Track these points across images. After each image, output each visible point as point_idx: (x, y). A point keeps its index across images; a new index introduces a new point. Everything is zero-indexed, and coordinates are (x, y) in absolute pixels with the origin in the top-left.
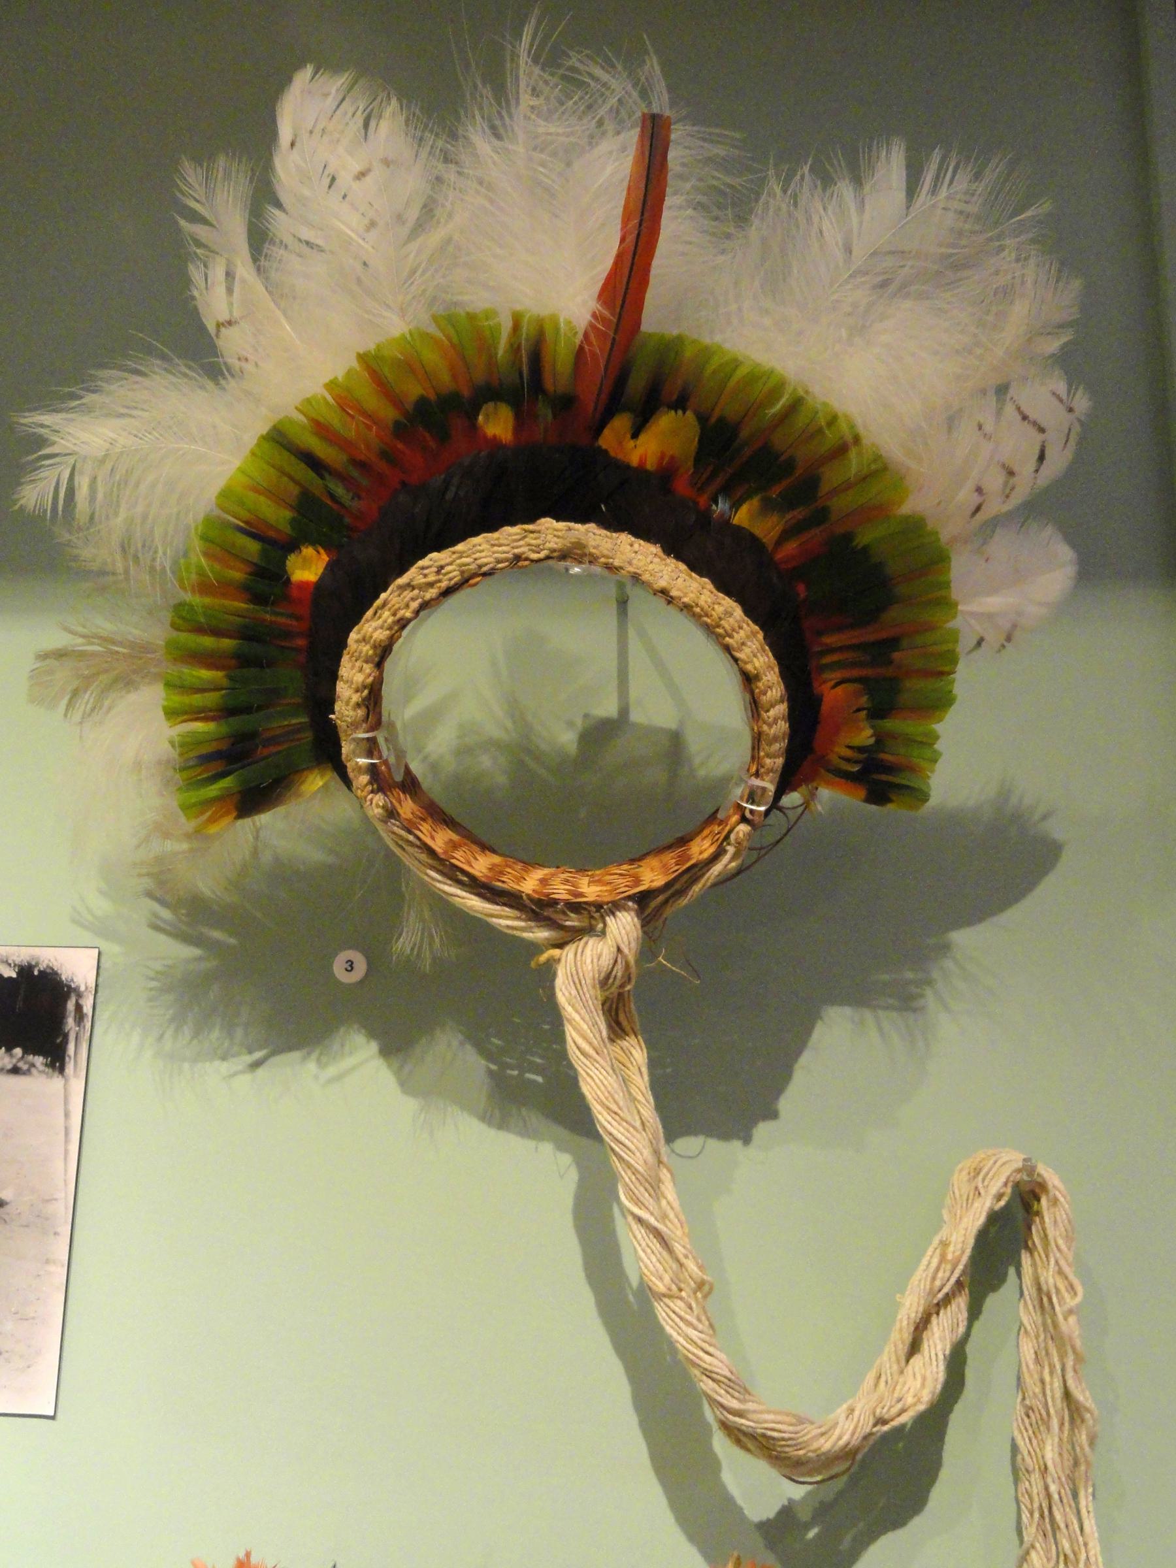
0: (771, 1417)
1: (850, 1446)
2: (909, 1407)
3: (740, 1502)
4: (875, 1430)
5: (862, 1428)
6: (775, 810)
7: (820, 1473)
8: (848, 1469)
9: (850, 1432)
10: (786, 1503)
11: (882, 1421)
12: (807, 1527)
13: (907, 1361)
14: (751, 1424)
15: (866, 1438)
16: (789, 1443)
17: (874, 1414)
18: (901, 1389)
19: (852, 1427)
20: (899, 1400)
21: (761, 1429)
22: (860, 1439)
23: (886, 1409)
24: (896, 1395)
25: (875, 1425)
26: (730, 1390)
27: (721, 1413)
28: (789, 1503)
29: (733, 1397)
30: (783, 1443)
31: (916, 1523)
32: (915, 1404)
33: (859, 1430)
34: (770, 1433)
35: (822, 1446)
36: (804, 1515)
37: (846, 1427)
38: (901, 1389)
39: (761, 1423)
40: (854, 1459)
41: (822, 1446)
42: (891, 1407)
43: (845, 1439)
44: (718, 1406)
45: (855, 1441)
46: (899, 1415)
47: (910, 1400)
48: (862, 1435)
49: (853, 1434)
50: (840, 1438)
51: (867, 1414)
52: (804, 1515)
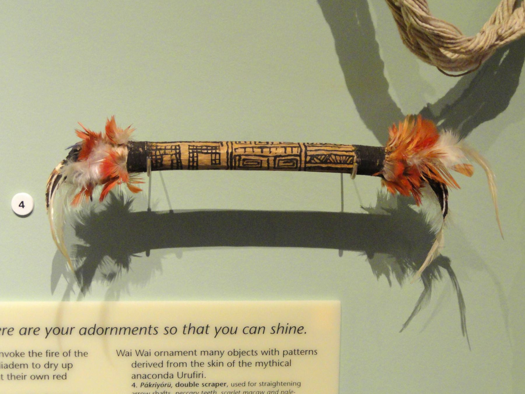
0: (443, 25)
1: (483, 49)
2: (517, 31)
3: (399, 105)
4: (496, 43)
5: (490, 40)
6: (163, 156)
7: (461, 70)
8: (477, 68)
9: (483, 41)
10: (426, 106)
11: (500, 38)
12: (437, 119)
13: (513, 10)
14: (432, 27)
15: (492, 46)
16: (452, 41)
17: (497, 33)
18: (512, 22)
19: (485, 38)
20: (510, 28)
21: (437, 31)
22: (488, 47)
23: (504, 31)
24: (509, 25)
25: (497, 40)
26: (422, 6)
27: (415, 21)
28: (428, 106)
29: (423, 10)
30: (449, 41)
31: (501, 116)
32: (520, 30)
33: (488, 41)
34: (442, 34)
35: (469, 46)
36: (437, 113)
37: (481, 39)
38: (512, 22)
39: (438, 28)
40: (480, 64)
41: (469, 46)
42: (506, 31)
43: (481, 44)
44: (413, 14)
45: (486, 47)
46: (510, 36)
47: (516, 27)
48: (490, 44)
49: (485, 42)
50: (478, 43)
51: (493, 33)
52: (437, 113)
